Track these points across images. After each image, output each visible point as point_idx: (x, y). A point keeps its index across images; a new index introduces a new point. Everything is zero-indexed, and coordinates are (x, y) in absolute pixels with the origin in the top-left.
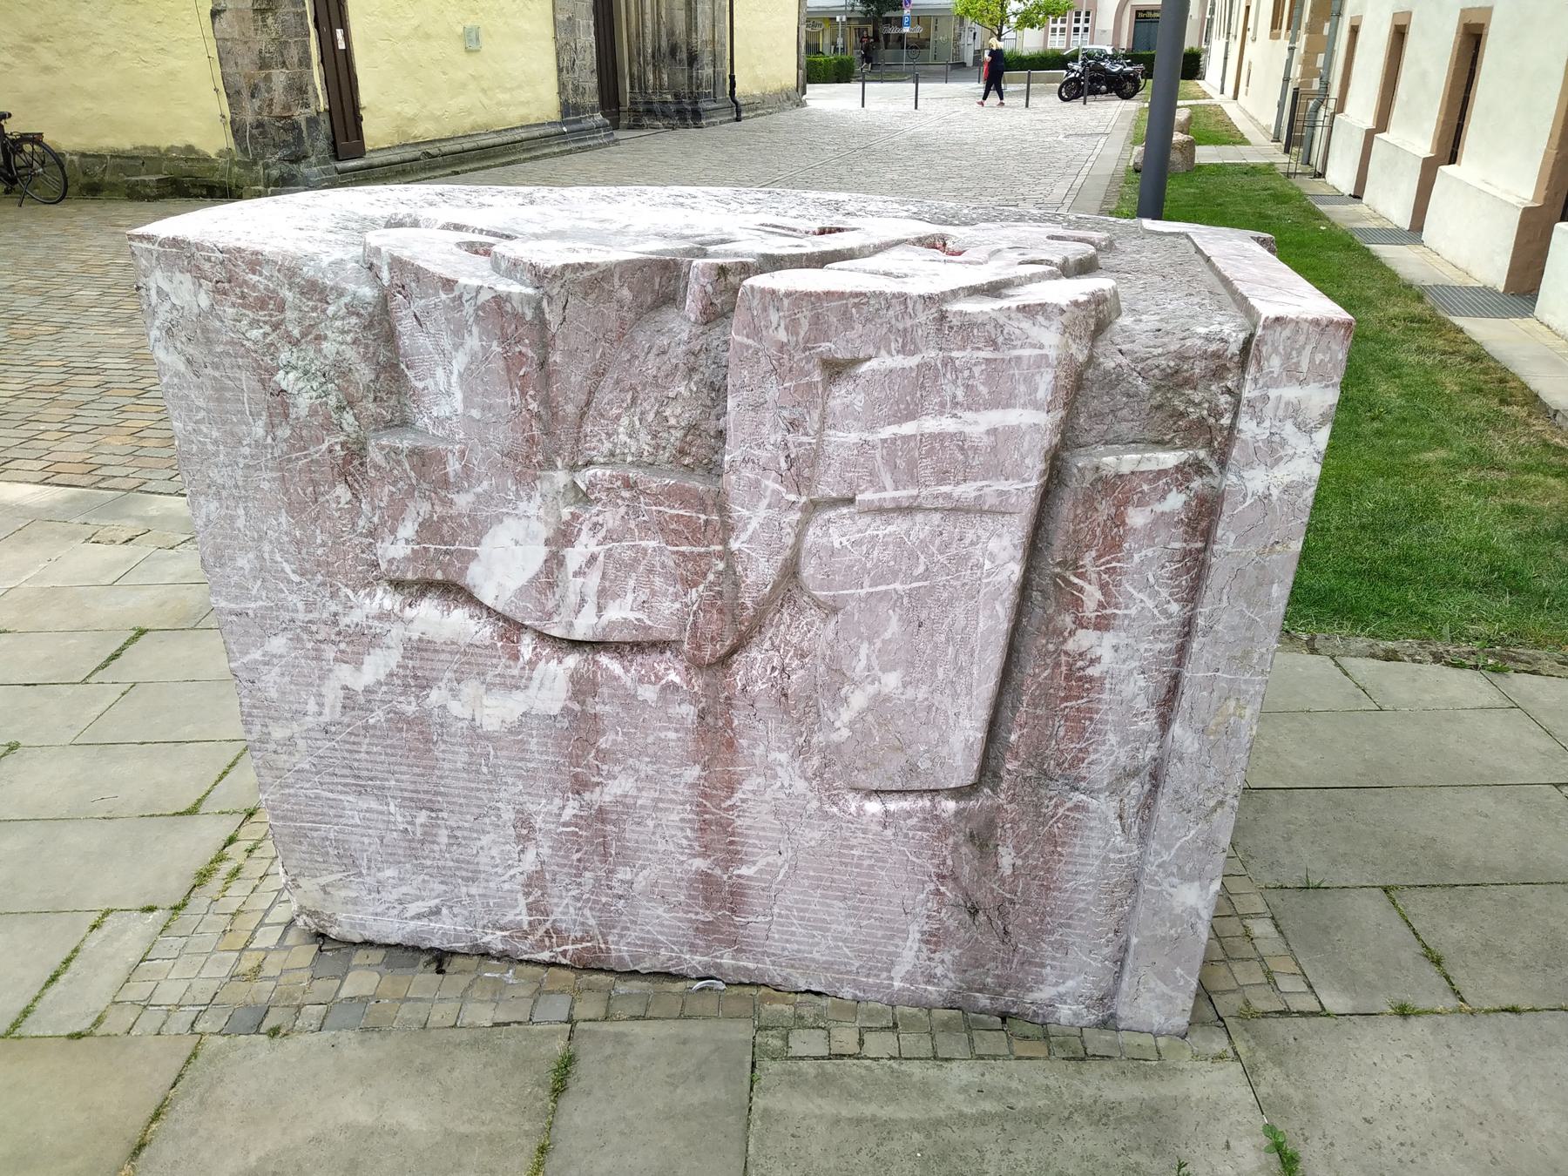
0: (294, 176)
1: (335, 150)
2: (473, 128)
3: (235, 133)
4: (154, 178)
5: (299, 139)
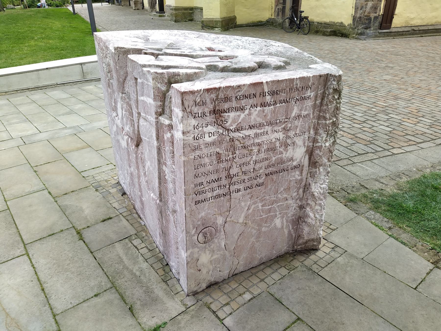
0: (364, 33)
1: (381, 27)
2: (436, 23)
3: (353, 19)
4: (330, 30)
5: (370, 22)
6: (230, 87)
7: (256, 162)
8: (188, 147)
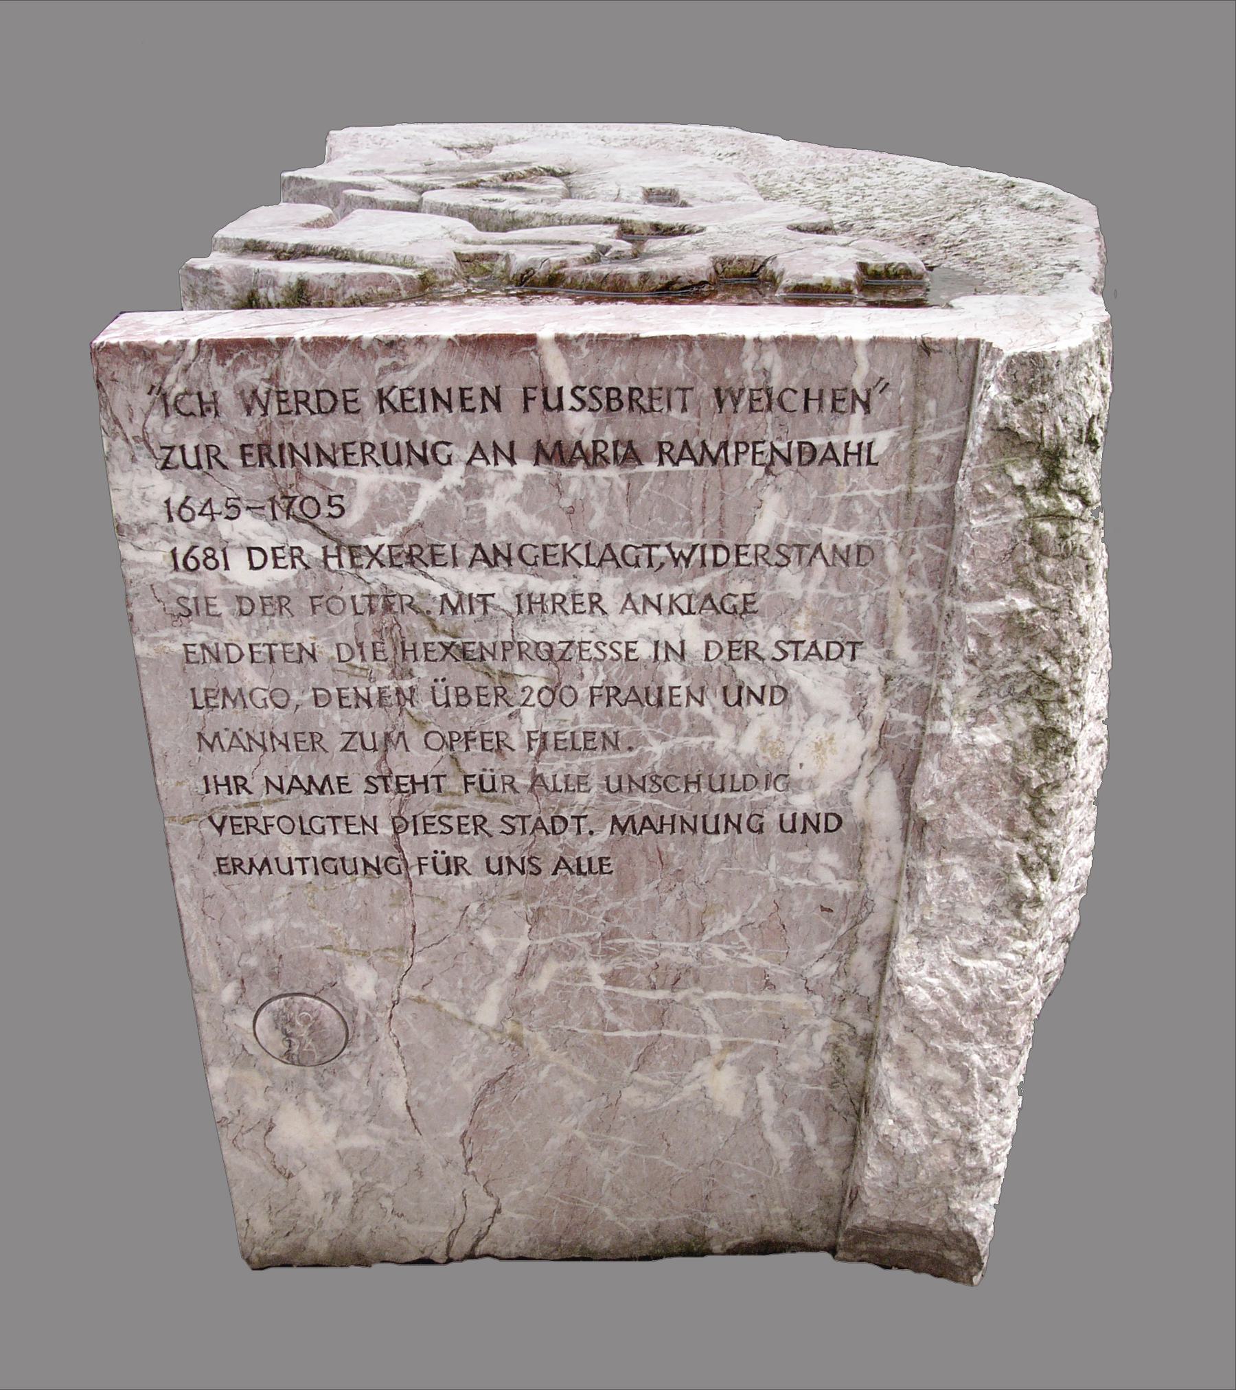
6: (343, 341)
7: (542, 742)
8: (150, 600)
